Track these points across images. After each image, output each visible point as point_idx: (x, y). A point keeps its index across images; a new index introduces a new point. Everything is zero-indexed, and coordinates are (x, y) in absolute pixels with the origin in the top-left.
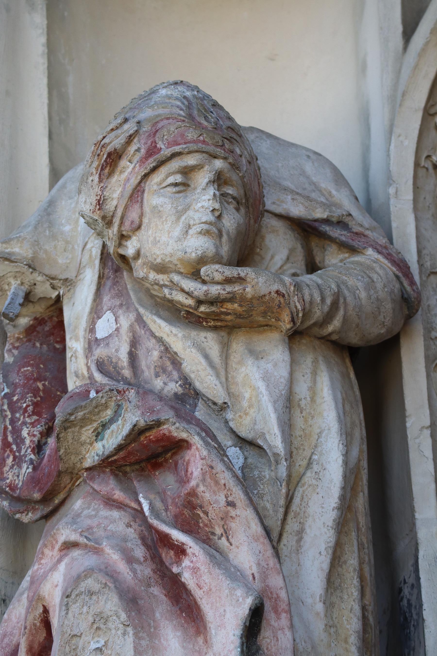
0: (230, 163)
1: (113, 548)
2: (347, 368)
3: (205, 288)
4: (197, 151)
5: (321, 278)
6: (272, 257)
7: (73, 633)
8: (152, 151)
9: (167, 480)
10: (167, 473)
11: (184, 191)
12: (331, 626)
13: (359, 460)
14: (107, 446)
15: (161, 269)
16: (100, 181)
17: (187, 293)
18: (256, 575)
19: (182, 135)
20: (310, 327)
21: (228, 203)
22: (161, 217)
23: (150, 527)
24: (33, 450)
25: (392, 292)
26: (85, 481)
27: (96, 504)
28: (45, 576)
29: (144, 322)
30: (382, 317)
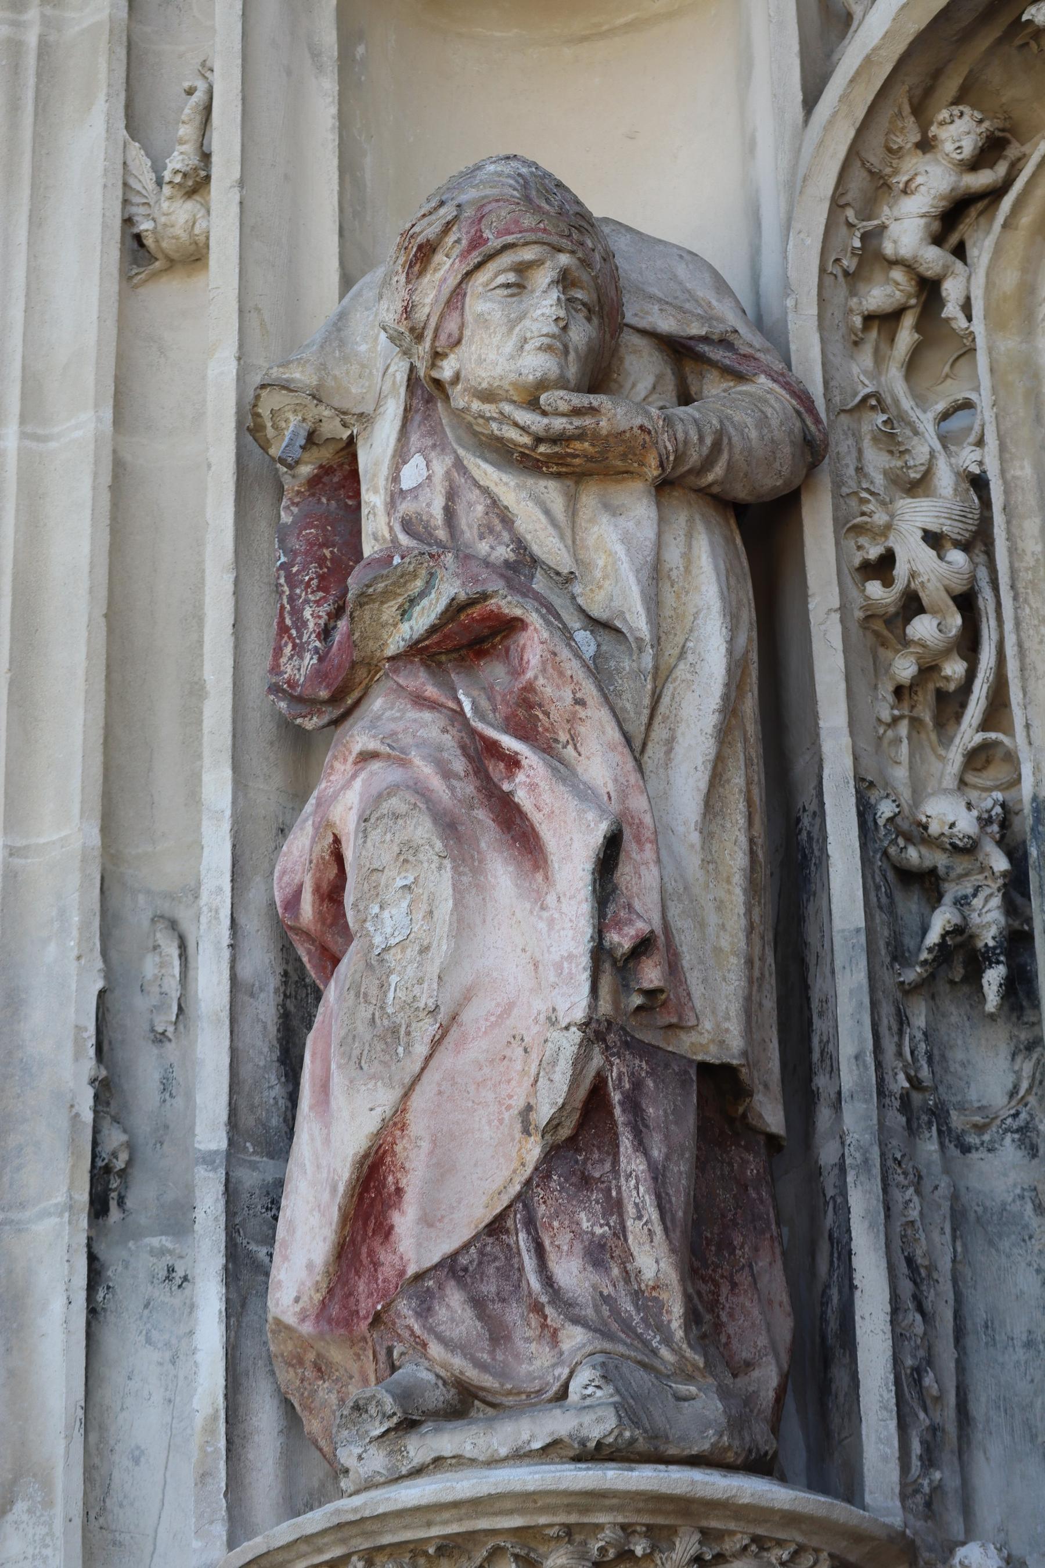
0: (579, 259)
1: (424, 758)
2: (731, 531)
3: (546, 421)
4: (535, 243)
5: (699, 411)
6: (634, 385)
7: (372, 867)
8: (477, 241)
9: (495, 672)
10: (496, 663)
11: (519, 294)
12: (709, 862)
13: (747, 652)
14: (415, 628)
15: (488, 396)
16: (408, 281)
17: (523, 428)
18: (612, 794)
19: (517, 222)
20: (683, 476)
21: (577, 311)
22: (487, 328)
23: (473, 732)
24: (318, 636)
25: (791, 432)
26: (386, 675)
27: (402, 703)
28: (335, 796)
29: (465, 467)
30: (777, 464)
